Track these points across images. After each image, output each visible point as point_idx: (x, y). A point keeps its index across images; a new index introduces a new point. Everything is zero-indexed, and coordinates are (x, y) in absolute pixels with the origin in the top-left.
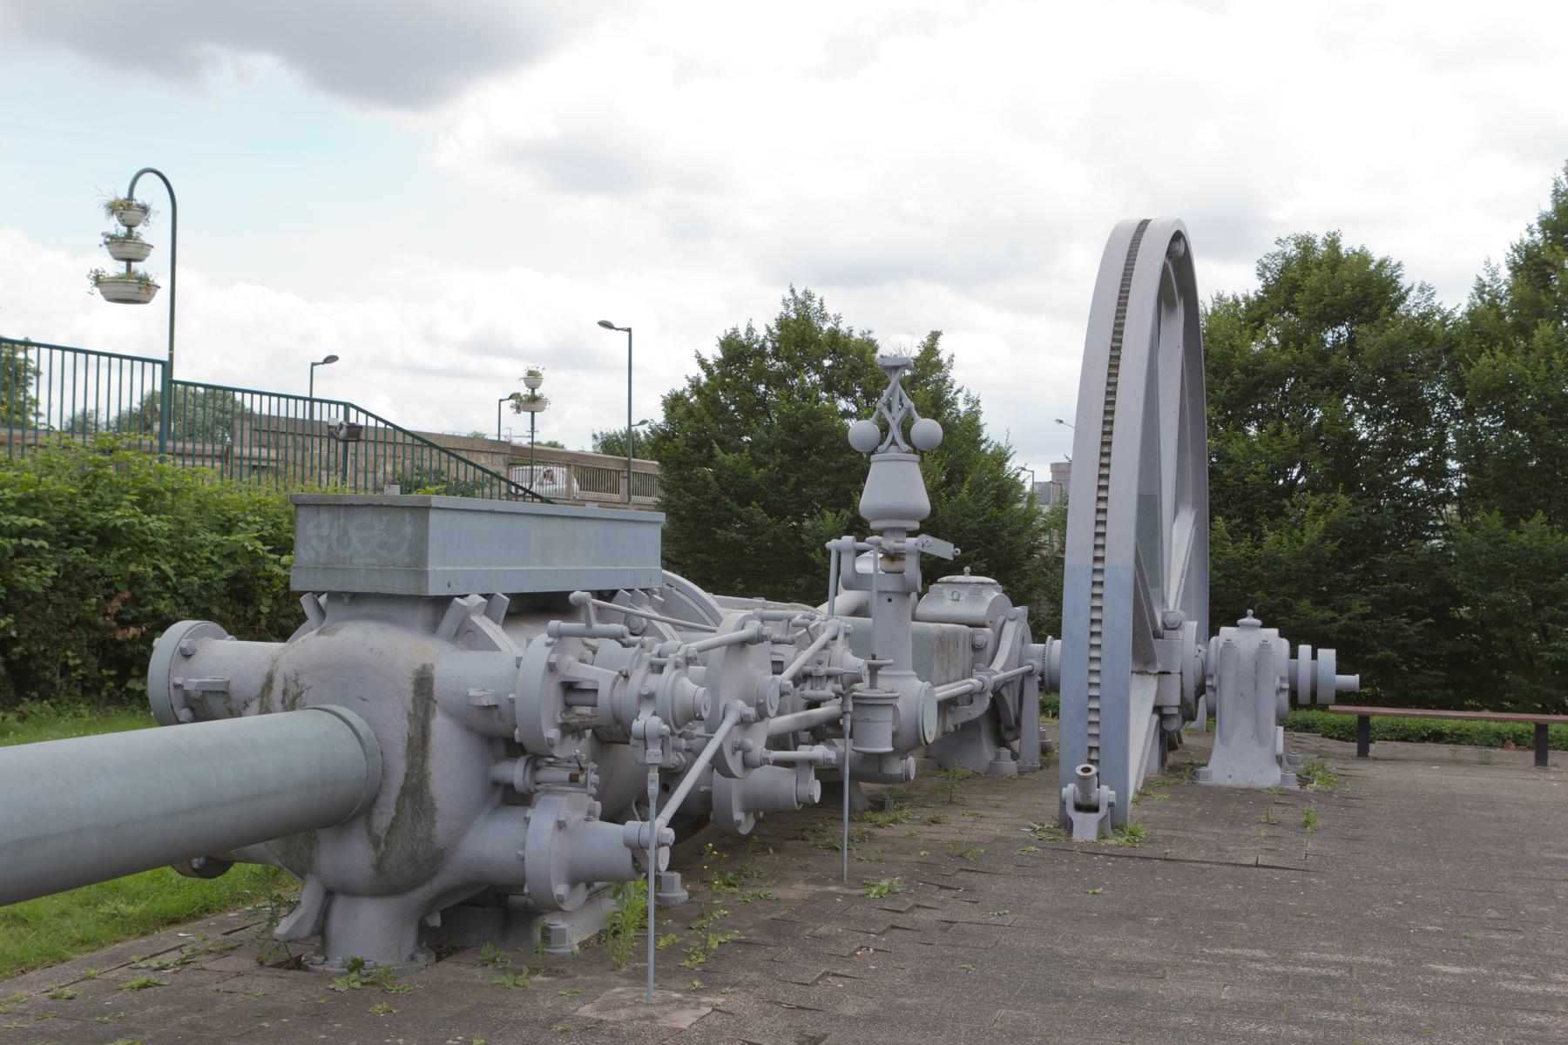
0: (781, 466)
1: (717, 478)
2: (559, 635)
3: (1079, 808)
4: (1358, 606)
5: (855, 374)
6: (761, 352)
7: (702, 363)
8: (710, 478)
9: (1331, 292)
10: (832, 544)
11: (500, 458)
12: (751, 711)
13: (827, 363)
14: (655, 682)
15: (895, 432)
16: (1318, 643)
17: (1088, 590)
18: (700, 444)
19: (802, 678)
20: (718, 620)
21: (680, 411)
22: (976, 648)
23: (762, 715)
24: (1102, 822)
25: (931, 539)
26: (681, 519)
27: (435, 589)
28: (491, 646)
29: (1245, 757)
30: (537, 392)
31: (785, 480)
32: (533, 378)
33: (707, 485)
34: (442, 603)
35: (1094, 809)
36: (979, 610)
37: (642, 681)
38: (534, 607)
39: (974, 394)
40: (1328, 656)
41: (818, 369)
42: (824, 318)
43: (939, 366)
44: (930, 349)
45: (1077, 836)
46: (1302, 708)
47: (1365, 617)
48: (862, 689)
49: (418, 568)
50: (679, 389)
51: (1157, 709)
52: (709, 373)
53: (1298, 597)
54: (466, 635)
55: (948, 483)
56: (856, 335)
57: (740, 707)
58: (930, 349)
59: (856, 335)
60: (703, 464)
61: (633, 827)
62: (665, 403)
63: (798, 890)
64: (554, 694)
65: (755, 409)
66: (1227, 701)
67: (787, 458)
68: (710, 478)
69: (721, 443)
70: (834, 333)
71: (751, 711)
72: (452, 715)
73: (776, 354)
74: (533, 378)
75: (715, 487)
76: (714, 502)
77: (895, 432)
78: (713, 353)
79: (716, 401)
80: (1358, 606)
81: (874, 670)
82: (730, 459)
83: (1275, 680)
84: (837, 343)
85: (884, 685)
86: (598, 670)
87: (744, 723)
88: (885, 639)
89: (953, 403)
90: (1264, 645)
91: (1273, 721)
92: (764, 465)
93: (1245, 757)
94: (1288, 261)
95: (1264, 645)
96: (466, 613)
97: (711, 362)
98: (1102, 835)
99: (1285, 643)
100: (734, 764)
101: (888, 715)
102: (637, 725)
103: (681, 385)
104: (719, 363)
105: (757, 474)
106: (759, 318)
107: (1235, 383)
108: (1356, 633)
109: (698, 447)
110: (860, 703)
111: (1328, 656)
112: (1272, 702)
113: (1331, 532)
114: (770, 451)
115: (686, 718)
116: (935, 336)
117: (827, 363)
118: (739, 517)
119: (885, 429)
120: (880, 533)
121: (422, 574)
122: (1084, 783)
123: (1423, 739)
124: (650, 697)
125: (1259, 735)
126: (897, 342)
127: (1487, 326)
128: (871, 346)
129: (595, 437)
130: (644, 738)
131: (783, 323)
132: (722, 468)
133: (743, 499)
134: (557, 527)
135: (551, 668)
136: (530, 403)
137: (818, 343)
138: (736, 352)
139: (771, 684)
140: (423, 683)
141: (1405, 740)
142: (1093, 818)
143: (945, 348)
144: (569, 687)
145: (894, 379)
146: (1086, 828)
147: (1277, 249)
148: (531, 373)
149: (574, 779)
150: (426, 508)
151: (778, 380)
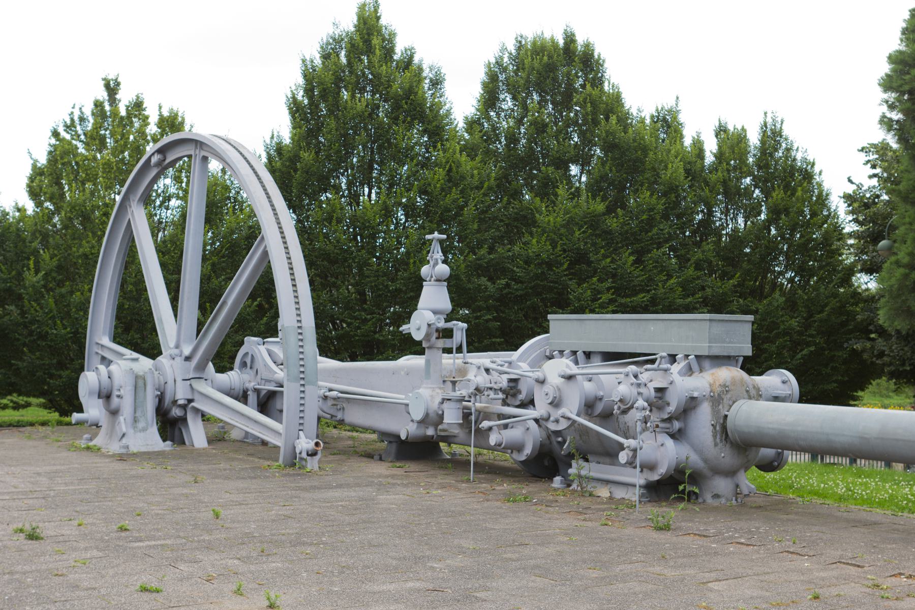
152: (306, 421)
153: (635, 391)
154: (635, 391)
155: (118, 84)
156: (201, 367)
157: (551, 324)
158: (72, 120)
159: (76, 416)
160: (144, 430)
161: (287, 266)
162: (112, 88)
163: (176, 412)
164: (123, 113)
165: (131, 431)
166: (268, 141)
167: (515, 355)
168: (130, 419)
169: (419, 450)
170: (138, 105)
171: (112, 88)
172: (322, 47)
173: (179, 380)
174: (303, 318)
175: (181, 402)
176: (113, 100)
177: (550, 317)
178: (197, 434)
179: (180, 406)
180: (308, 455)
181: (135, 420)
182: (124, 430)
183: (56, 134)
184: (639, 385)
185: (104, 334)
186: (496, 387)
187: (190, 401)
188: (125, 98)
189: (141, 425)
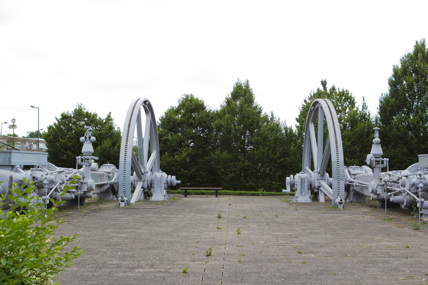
0: (75, 142)
1: (60, 145)
2: (32, 170)
3: (121, 201)
4: (193, 170)
5: (92, 122)
6: (70, 117)
7: (57, 119)
8: (58, 145)
9: (191, 107)
10: (77, 157)
11: (5, 140)
12: (62, 182)
13: (86, 119)
14: (47, 176)
15: (88, 139)
16: (172, 175)
17: (123, 165)
18: (56, 137)
19: (70, 179)
20: (56, 169)
21: (51, 130)
22: (109, 177)
23: (63, 183)
24: (125, 203)
25: (93, 156)
26: (52, 154)
27: (12, 164)
28: (21, 172)
29: (159, 195)
30: (15, 124)
31: (76, 145)
32: (14, 120)
33: (58, 147)
34: (13, 166)
35: (124, 201)
36: (110, 170)
37: (45, 176)
38: (26, 168)
39: (119, 126)
40: (174, 177)
41: (84, 121)
42: (85, 109)
43: (111, 120)
44: (109, 116)
45: (121, 206)
46: (171, 188)
47: (194, 172)
48: (82, 181)
49: (10, 161)
50: (51, 125)
51: (142, 187)
52: (58, 121)
53: (181, 168)
54: (17, 171)
55: (113, 146)
56: (92, 113)
57: (60, 181)
58: (109, 116)
59: (92, 113)
60: (57, 142)
61: (43, 197)
62: (48, 128)
63: (71, 212)
64: (31, 178)
65: (69, 129)
66: (155, 185)
67: (76, 140)
68: (58, 145)
69: (61, 137)
70: (87, 113)
71: (62, 182)
72: (16, 182)
73: (74, 117)
74: (14, 120)
75: (60, 147)
76: (59, 150)
77: (88, 139)
78: (59, 117)
79: (60, 128)
80: (193, 170)
81: (84, 178)
82: (63, 141)
83: (164, 182)
84: (88, 115)
85: (85, 180)
86: (38, 174)
87: (61, 184)
88: (90, 174)
89: (114, 128)
90: (162, 175)
91: (164, 188)
92: (71, 142)
93: (159, 195)
94: (184, 99)
95: (162, 175)
96: (17, 168)
97: (59, 119)
98: (125, 206)
99: (166, 175)
100: (59, 190)
101: (86, 185)
102: (44, 182)
103: (52, 124)
104: (61, 119)
105: (69, 144)
106: (70, 110)
107: (171, 125)
108: (193, 175)
109: (56, 138)
110: (81, 183)
111: (174, 177)
112: (163, 186)
113: (188, 155)
114: (72, 139)
115: (52, 182)
116: (110, 113)
117: (86, 119)
118: (65, 153)
119: (86, 138)
120: (85, 155)
121: (10, 162)
122: (122, 197)
123: (200, 194)
124: (46, 178)
125: (161, 192)
126: (102, 116)
127: (219, 115)
128: (96, 115)
129: (28, 132)
130: (45, 184)
131: (75, 110)
132: (61, 143)
133: (66, 150)
134: (30, 155)
135: (31, 175)
136: (13, 126)
137: (83, 115)
138: (65, 117)
139: (65, 179)
140: (11, 178)
141: (197, 194)
142: (124, 203)
143: (112, 117)
144: (34, 178)
145: (87, 130)
146: (122, 204)
147: (182, 97)
148: (13, 119)
149: (34, 191)
150: (11, 152)
151: (75, 123)
152: (340, 193)
153: (419, 181)
154: (419, 181)
155: (326, 82)
156: (323, 175)
157: (420, 159)
158: (311, 96)
159: (284, 190)
160: (304, 196)
161: (335, 141)
162: (324, 84)
163: (316, 190)
164: (328, 91)
165: (300, 196)
166: (381, 96)
167: (406, 170)
168: (299, 192)
169: (389, 206)
170: (334, 89)
171: (324, 84)
172: (401, 60)
173: (316, 180)
174: (339, 158)
175: (316, 187)
176: (325, 88)
177: (419, 155)
178: (322, 198)
179: (316, 188)
180: (339, 204)
181: (301, 193)
182: (297, 195)
183: (305, 101)
184: (421, 179)
185: (307, 166)
186: (391, 180)
187: (320, 187)
188: (329, 87)
189: (303, 194)
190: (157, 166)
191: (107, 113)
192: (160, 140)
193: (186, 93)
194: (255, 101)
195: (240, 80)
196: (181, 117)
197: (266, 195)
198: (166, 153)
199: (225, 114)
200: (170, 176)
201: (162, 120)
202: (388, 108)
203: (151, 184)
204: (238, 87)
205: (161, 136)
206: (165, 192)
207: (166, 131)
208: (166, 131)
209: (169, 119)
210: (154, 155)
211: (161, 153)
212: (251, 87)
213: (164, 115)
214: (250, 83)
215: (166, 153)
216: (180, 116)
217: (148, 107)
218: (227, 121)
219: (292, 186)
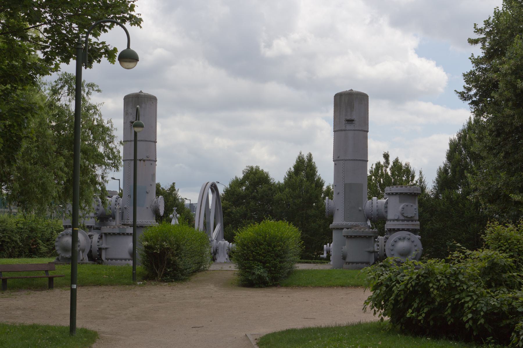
9: (256, 178)
66: (220, 251)
116: (174, 183)
127: (280, 188)
190: (221, 235)
191: (171, 184)
192: (224, 212)
193: (250, 165)
194: (318, 174)
195: (302, 154)
196: (245, 189)
197: (317, 263)
198: (230, 225)
199: (285, 188)
200: (231, 244)
201: (227, 191)
202: (445, 180)
203: (216, 250)
204: (300, 160)
205: (225, 208)
206: (227, 256)
207: (230, 203)
208: (230, 203)
209: (234, 192)
210: (218, 227)
211: (225, 225)
212: (313, 160)
213: (229, 187)
214: (313, 156)
215: (230, 225)
216: (244, 188)
217: (214, 188)
218: (287, 196)
219: (328, 252)
